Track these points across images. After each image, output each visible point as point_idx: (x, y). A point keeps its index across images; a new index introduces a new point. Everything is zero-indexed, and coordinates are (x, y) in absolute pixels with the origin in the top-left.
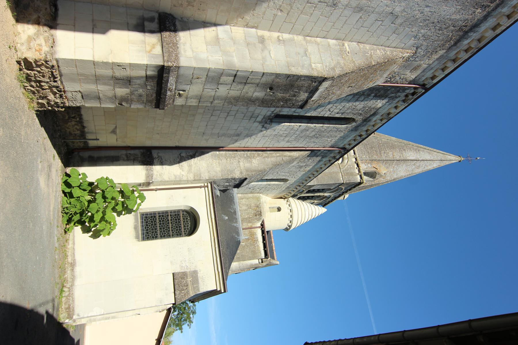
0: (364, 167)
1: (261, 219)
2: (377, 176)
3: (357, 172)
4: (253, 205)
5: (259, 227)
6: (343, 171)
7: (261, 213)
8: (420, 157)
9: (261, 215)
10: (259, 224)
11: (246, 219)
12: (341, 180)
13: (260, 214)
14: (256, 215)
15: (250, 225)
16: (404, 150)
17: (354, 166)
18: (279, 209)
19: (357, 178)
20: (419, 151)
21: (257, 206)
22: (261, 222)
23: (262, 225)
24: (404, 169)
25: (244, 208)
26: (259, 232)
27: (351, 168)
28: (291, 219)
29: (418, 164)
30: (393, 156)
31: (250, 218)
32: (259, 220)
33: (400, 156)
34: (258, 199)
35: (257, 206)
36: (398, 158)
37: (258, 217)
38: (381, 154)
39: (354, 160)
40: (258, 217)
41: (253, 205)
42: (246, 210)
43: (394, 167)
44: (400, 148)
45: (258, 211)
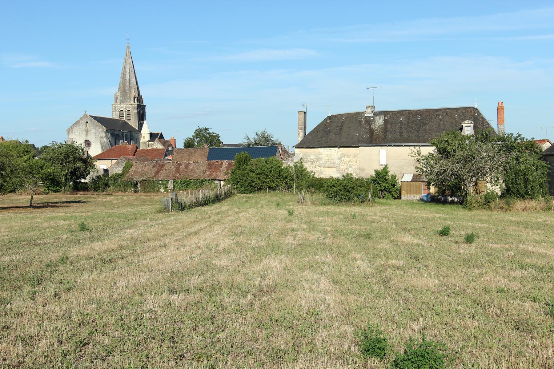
10: (148, 142)
16: (126, 79)
23: (148, 141)
29: (131, 72)
38: (127, 92)
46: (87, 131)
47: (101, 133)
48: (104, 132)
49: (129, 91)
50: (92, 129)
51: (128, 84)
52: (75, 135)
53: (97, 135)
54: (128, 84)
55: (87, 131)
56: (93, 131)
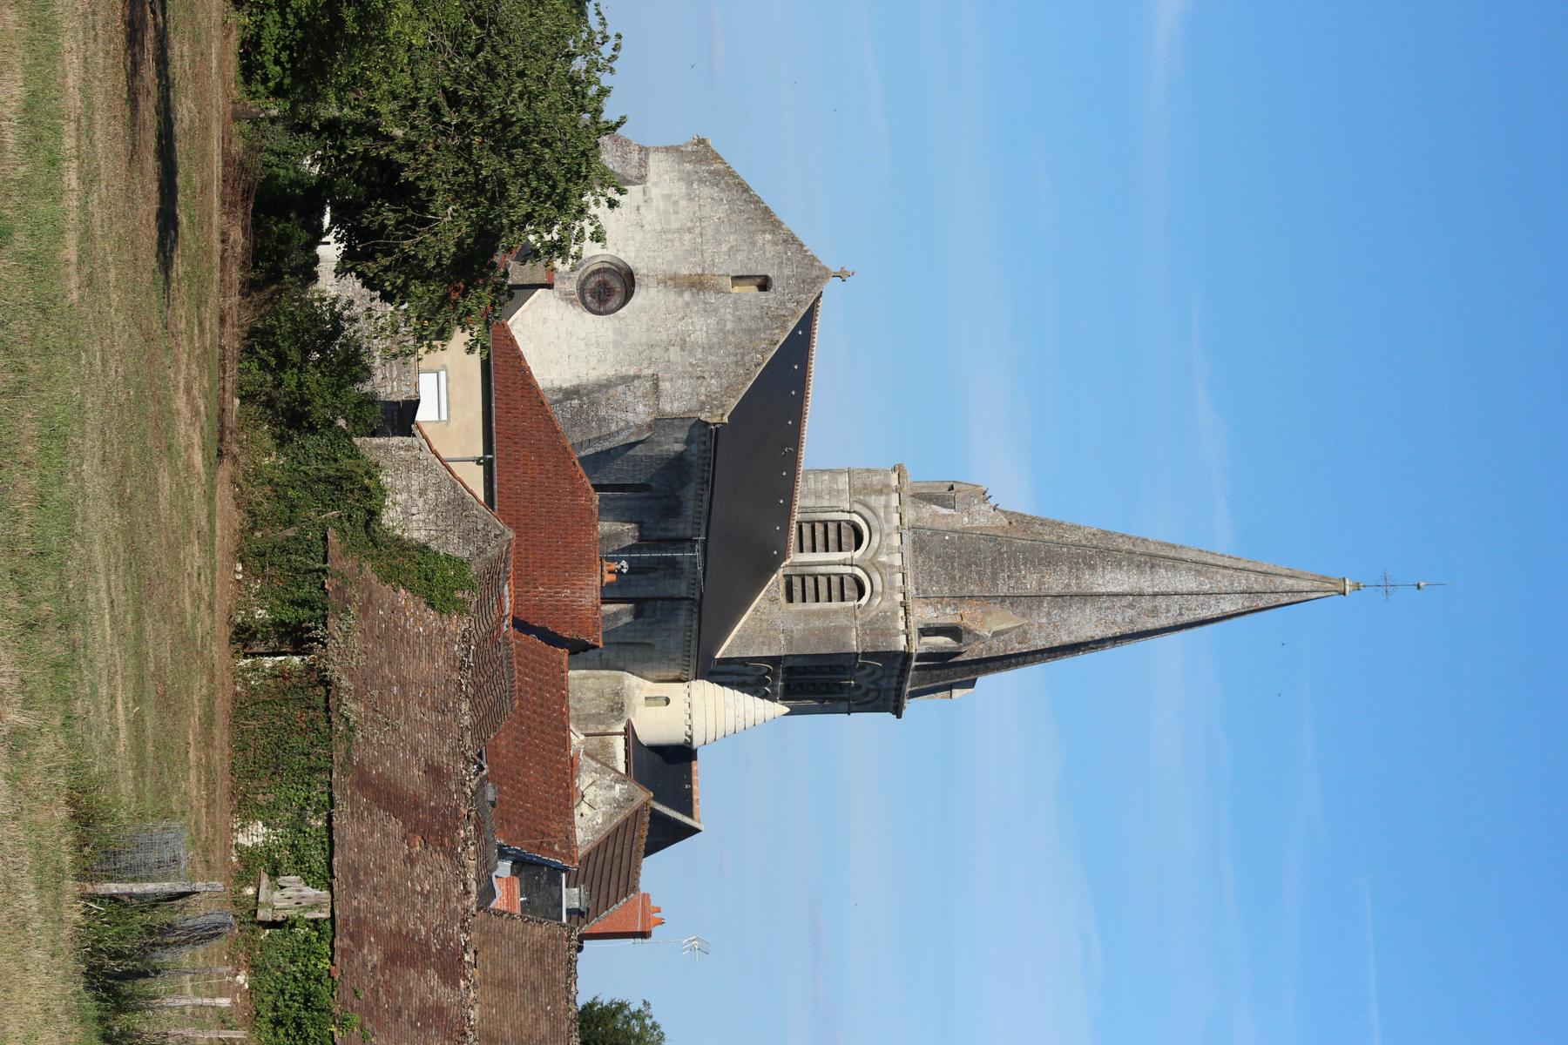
0: (926, 614)
1: (622, 718)
2: (965, 636)
3: (901, 625)
4: (607, 690)
5: (620, 734)
6: (863, 625)
7: (623, 705)
8: (1153, 586)
9: (623, 710)
10: (620, 728)
11: (593, 715)
12: (852, 646)
13: (621, 709)
14: (612, 711)
15: (601, 728)
16: (1092, 568)
17: (896, 613)
18: (668, 701)
19: (898, 642)
20: (1152, 567)
21: (617, 694)
22: (624, 724)
23: (629, 732)
24: (1094, 619)
25: (590, 695)
26: (619, 744)
27: (885, 618)
28: (689, 711)
29: (1146, 604)
30: (1041, 583)
31: (600, 714)
32: (619, 719)
33: (1068, 585)
34: (620, 680)
35: (617, 694)
36: (1057, 589)
37: (616, 713)
39: (900, 597)
40: (616, 713)
41: (607, 690)
42: (593, 699)
43: (1049, 613)
44: (1078, 563)
45: (617, 703)
46: (697, 284)
47: (685, 386)
48: (694, 404)
49: (1002, 589)
50: (712, 321)
51: (1056, 582)
52: (667, 197)
53: (675, 354)
54: (1056, 582)
55: (697, 284)
56: (701, 328)
